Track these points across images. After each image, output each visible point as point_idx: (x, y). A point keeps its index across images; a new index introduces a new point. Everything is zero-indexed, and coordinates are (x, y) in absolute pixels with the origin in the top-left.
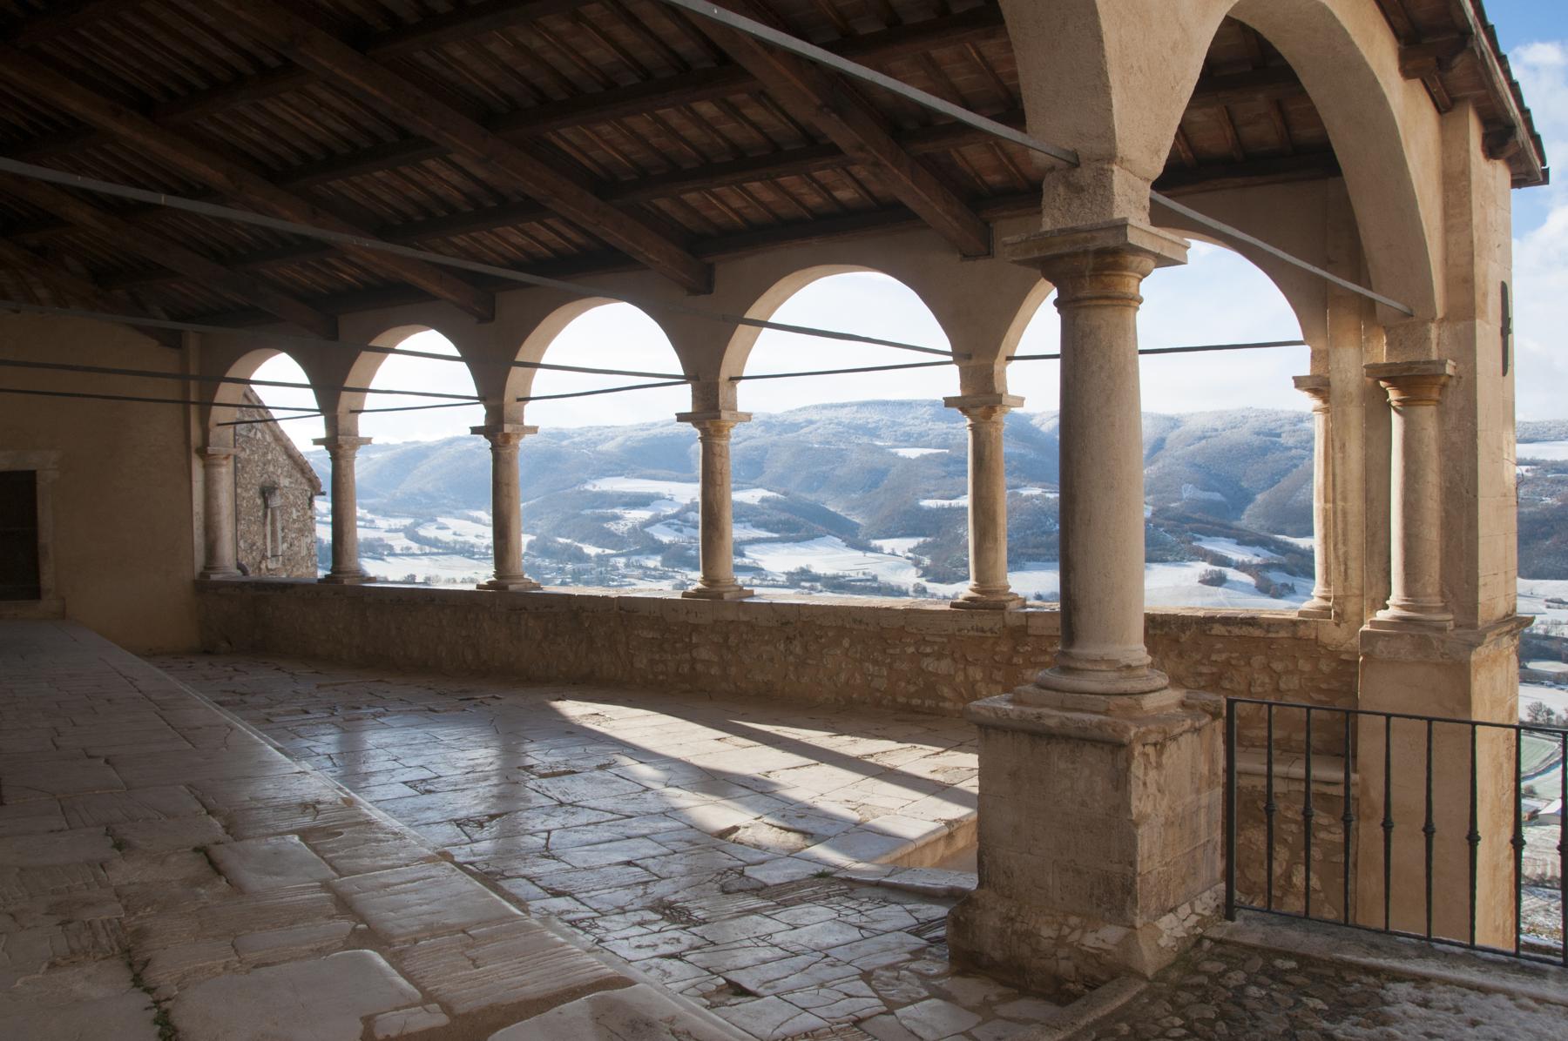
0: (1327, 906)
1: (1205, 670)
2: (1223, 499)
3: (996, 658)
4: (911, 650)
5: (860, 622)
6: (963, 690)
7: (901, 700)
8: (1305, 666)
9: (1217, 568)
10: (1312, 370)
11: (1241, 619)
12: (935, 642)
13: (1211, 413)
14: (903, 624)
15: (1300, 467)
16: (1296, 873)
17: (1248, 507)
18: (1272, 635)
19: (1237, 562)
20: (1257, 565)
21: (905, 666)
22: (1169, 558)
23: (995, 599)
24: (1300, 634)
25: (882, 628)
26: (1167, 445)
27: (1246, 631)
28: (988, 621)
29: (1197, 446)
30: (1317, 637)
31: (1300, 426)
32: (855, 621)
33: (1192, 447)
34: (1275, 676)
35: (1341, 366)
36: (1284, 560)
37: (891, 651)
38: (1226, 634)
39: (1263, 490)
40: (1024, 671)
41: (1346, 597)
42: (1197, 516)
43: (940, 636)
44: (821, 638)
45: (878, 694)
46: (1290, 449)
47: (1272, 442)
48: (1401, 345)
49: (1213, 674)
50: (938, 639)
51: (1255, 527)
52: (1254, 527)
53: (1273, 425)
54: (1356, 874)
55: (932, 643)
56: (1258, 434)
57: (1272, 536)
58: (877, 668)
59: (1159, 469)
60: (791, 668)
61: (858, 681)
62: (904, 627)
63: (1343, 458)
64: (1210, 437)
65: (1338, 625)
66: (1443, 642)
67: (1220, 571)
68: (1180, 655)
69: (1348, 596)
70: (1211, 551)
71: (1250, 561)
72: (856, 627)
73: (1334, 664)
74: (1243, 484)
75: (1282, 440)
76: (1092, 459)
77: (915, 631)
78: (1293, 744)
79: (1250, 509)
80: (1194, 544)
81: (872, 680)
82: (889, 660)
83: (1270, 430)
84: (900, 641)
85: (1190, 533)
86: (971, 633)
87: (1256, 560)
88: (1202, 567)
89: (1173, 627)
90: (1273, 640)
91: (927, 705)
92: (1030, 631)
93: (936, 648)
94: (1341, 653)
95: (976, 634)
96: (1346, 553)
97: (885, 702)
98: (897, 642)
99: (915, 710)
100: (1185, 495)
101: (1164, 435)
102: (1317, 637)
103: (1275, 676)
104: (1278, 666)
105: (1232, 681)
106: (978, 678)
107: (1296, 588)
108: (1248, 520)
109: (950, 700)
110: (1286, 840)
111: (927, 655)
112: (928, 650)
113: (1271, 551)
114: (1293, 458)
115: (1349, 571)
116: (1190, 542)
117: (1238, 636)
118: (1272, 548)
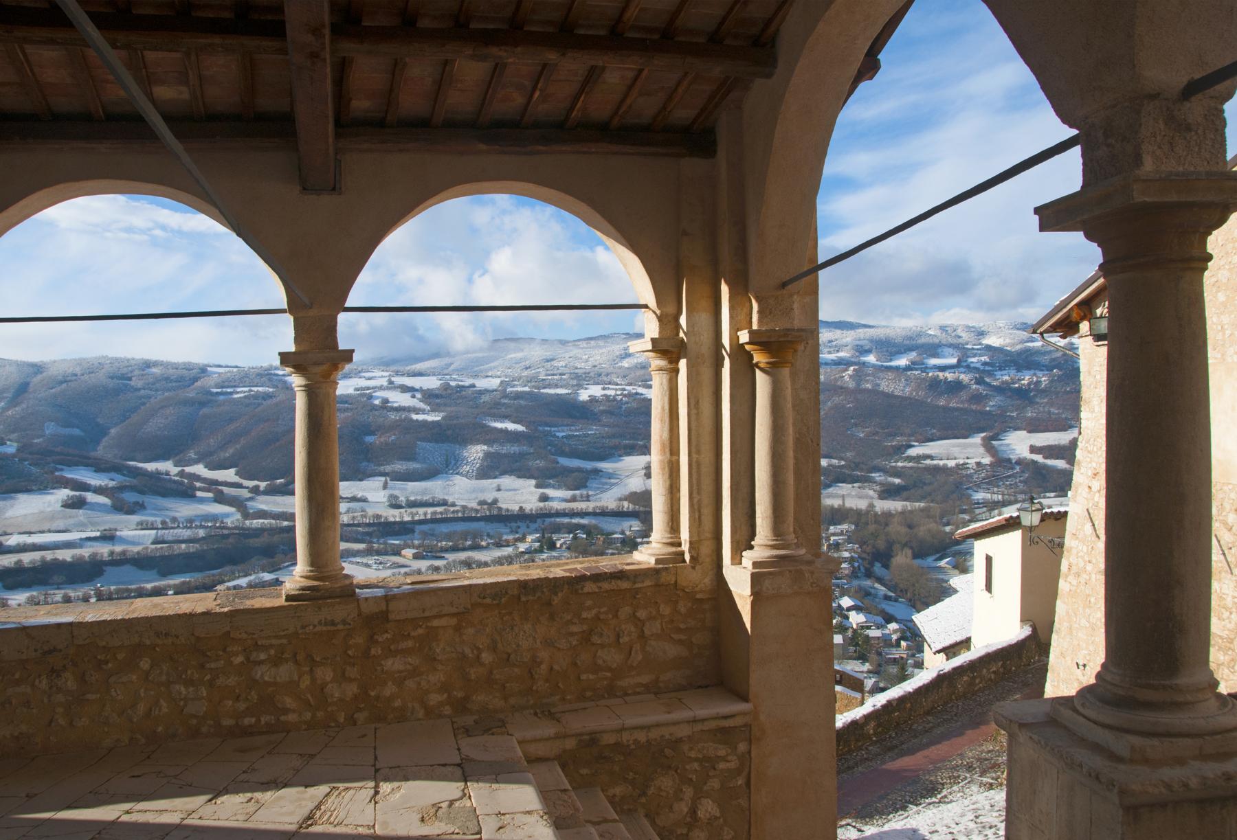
0: (726, 828)
1: (575, 629)
2: (82, 434)
3: (350, 652)
4: (239, 659)
5: (167, 635)
6: (309, 696)
7: (227, 722)
8: (666, 610)
9: (77, 493)
10: (660, 333)
11: (611, 573)
12: (271, 646)
13: (71, 360)
14: (228, 629)
15: (148, 405)
16: (700, 807)
17: (104, 440)
18: (637, 586)
19: (96, 487)
20: (113, 488)
21: (232, 681)
22: (34, 488)
23: (339, 585)
24: (663, 580)
25: (198, 639)
26: (31, 389)
27: (615, 585)
28: (340, 612)
29: (59, 389)
30: (676, 581)
31: (148, 371)
32: (158, 635)
33: (54, 390)
34: (640, 624)
35: (696, 329)
36: (135, 481)
37: (213, 665)
38: (597, 590)
39: (116, 425)
40: (383, 662)
41: (700, 541)
42: (58, 449)
43: (276, 637)
44: (107, 662)
45: (194, 721)
46: (139, 390)
47: (124, 384)
48: (770, 313)
49: (584, 632)
50: (274, 642)
51: (110, 456)
52: (109, 456)
53: (125, 370)
54: (750, 793)
55: (265, 648)
56: (112, 378)
57: (124, 462)
58: (191, 689)
59: (23, 410)
60: (60, 710)
61: (165, 710)
62: (229, 632)
63: (697, 414)
64: (70, 381)
65: (693, 568)
66: (812, 573)
67: (80, 495)
68: (552, 617)
69: (701, 540)
70: (72, 479)
71: (106, 485)
72: (159, 642)
73: (690, 604)
74: (99, 420)
75: (132, 383)
76: (1201, 451)
77: (244, 636)
78: (661, 685)
79: (105, 441)
80: (57, 474)
81: (185, 705)
82: (208, 677)
83: (123, 374)
84: (224, 650)
85: (52, 465)
86: (318, 628)
87: (112, 484)
88: (64, 493)
89: (545, 590)
90: (638, 591)
91: (263, 722)
92: (392, 617)
93: (272, 652)
94: (696, 593)
95: (324, 628)
96: (700, 501)
97: (204, 729)
98: (221, 653)
99: (247, 732)
100: (47, 432)
101: (28, 379)
102: (676, 581)
103: (640, 624)
104: (642, 614)
105: (601, 635)
106: (328, 679)
107: (146, 504)
108: (102, 451)
109: (294, 711)
110: (691, 779)
111: (261, 662)
112: (263, 656)
113: (124, 475)
114: (141, 398)
115: (703, 517)
116: (52, 473)
117: (607, 591)
118: (125, 472)
